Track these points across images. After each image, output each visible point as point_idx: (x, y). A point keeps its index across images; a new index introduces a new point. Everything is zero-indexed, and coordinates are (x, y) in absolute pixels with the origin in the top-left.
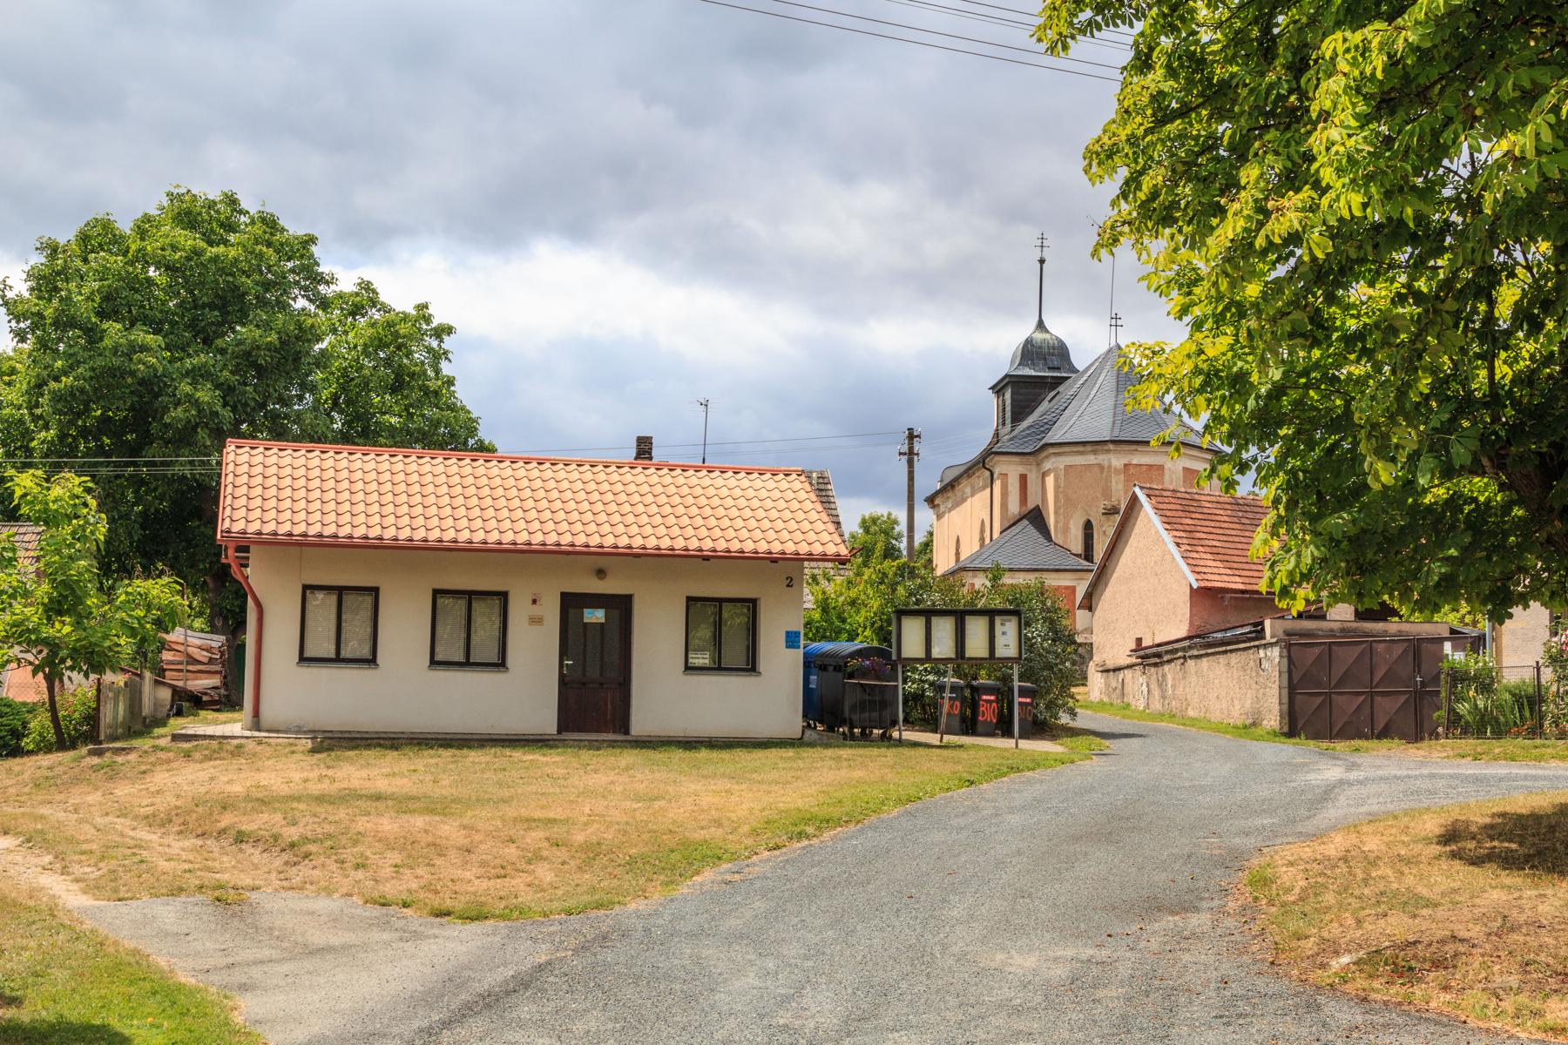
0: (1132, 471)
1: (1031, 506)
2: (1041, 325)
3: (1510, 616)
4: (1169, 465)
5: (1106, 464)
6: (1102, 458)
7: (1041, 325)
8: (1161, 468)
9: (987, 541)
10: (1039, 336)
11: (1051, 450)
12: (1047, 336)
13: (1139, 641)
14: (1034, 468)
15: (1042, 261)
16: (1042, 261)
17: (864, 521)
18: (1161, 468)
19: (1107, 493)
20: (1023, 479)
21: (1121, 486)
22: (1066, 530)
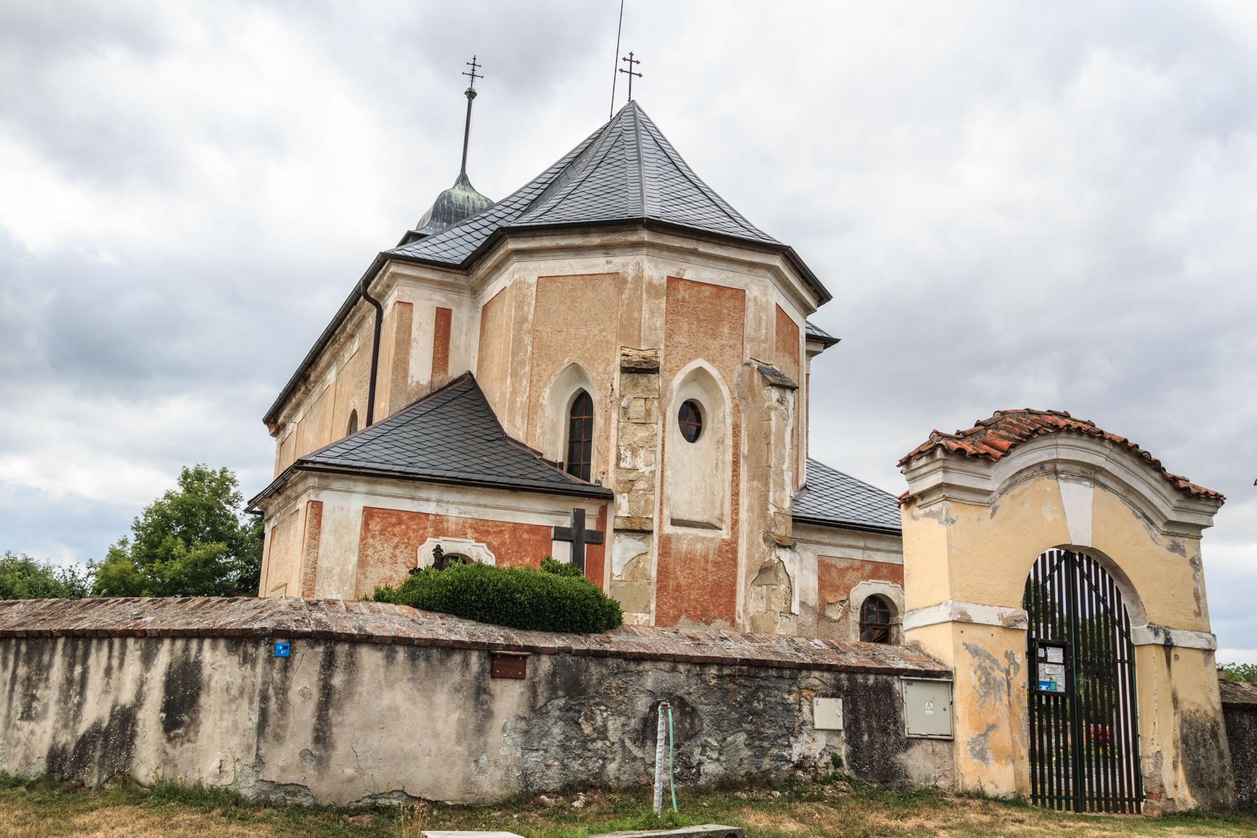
0: (682, 293)
1: (454, 371)
2: (463, 179)
3: (162, 711)
4: (753, 292)
5: (630, 272)
6: (624, 263)
7: (463, 179)
8: (739, 294)
9: (361, 425)
10: (460, 194)
11: (512, 245)
12: (472, 195)
13: (993, 514)
14: (466, 299)
15: (471, 94)
16: (471, 94)
17: (186, 475)
18: (739, 294)
19: (629, 331)
20: (443, 318)
21: (659, 322)
22: (532, 409)
